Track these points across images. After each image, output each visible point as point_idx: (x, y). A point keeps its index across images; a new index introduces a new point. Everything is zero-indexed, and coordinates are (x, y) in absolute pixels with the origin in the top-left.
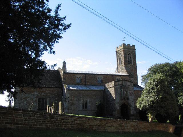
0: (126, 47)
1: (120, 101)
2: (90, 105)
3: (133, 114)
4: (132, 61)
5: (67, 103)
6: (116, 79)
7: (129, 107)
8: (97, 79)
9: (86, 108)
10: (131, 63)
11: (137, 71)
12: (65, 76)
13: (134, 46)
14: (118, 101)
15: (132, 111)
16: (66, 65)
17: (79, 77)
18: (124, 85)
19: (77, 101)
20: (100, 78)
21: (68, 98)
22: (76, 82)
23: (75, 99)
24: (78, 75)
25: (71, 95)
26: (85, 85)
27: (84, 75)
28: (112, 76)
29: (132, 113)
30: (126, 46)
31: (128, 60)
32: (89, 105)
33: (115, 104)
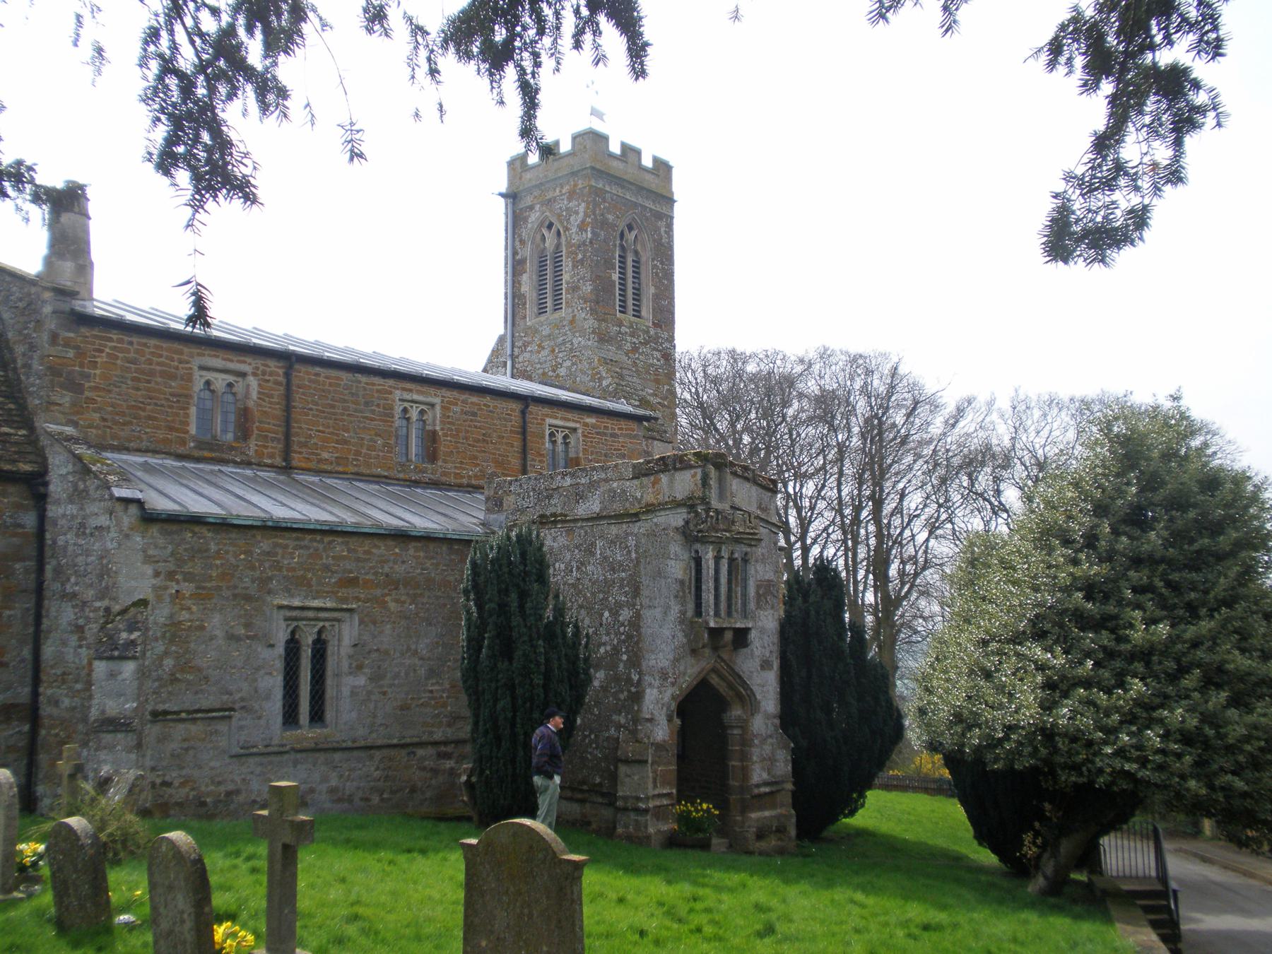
0: (615, 163)
1: (676, 660)
2: (361, 681)
3: (766, 784)
4: (649, 291)
5: (129, 668)
6: (398, 409)
7: (736, 712)
8: (388, 414)
9: (317, 716)
10: (637, 313)
11: (489, 352)
12: (81, 354)
13: (663, 169)
14: (666, 664)
15: (755, 754)
16: (86, 232)
17: (220, 381)
18: (715, 503)
19: (231, 637)
20: (414, 414)
21: (143, 603)
22: (193, 430)
23: (215, 623)
24: (218, 363)
25: (171, 575)
26: (287, 468)
27: (273, 364)
28: (516, 406)
29: (758, 775)
30: (645, 170)
31: (616, 277)
32: (346, 686)
33: (637, 697)
